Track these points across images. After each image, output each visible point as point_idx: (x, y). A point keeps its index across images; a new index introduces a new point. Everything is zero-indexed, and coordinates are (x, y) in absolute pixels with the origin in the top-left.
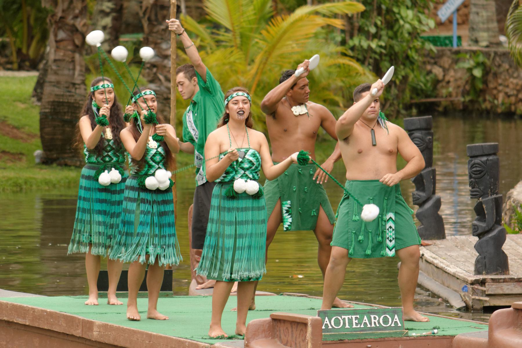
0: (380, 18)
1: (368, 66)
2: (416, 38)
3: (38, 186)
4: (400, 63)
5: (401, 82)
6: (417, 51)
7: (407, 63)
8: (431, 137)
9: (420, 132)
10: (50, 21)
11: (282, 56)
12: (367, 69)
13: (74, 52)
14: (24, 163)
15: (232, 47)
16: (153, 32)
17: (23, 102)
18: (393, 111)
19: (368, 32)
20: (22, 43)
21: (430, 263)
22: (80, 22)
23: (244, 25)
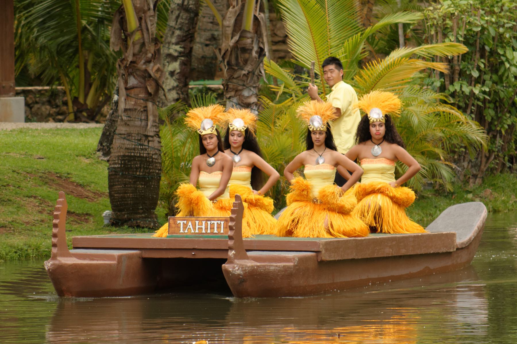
0: (483, 60)
13: (147, 100)
14: (91, 225)
19: (471, 76)
20: (78, 91)
22: (153, 67)
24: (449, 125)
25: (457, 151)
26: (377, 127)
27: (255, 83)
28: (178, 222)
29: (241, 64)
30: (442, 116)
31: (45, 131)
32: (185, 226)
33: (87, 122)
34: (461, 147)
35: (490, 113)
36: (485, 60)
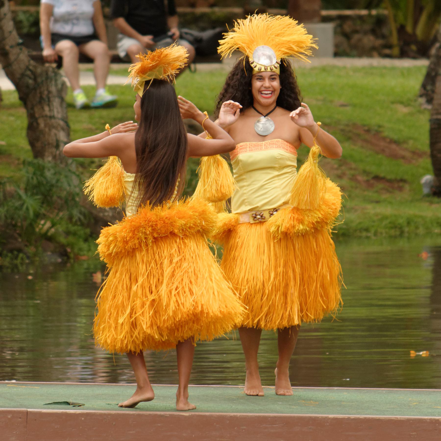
14: (406, 194)
17: (406, 104)
20: (406, 18)
26: (267, 80)
31: (356, 70)
33: (414, 58)
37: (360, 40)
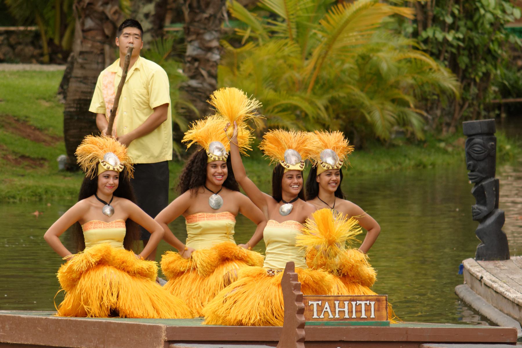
0: (457, 6)
1: (443, 61)
2: (499, 30)
3: (61, 196)
4: (480, 57)
5: (481, 79)
6: (501, 45)
7: (489, 58)
8: (493, 143)
9: (481, 137)
10: (77, 7)
11: (345, 49)
12: (442, 64)
13: (103, 43)
14: (46, 170)
15: (286, 38)
16: (195, 21)
17: (48, 101)
18: (472, 113)
19: (444, 22)
20: (54, 33)
21: (489, 287)
22: (111, 9)
23: (300, 13)
24: (421, 72)
25: (429, 99)
26: (219, 168)
27: (217, 26)
28: (310, 303)
29: (203, 7)
30: (414, 63)
31: (12, 73)
32: (320, 308)
34: (434, 94)
35: (464, 61)
36: (460, 6)
37: (22, 50)
